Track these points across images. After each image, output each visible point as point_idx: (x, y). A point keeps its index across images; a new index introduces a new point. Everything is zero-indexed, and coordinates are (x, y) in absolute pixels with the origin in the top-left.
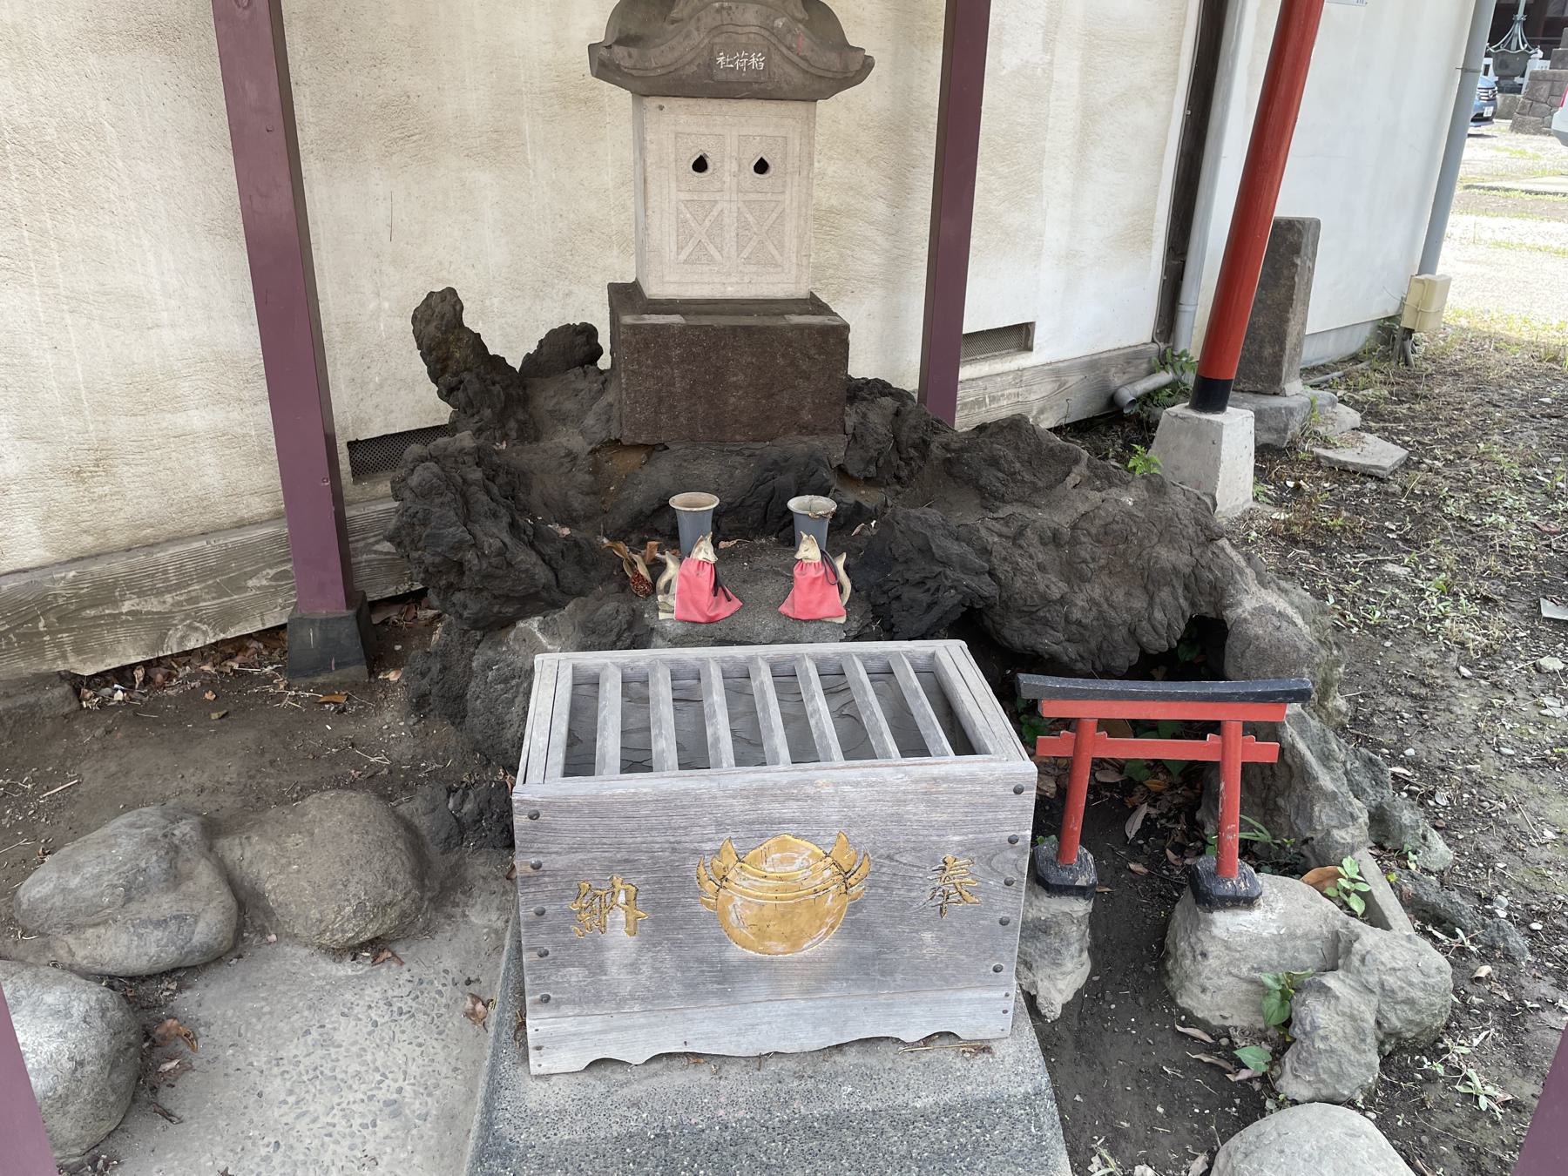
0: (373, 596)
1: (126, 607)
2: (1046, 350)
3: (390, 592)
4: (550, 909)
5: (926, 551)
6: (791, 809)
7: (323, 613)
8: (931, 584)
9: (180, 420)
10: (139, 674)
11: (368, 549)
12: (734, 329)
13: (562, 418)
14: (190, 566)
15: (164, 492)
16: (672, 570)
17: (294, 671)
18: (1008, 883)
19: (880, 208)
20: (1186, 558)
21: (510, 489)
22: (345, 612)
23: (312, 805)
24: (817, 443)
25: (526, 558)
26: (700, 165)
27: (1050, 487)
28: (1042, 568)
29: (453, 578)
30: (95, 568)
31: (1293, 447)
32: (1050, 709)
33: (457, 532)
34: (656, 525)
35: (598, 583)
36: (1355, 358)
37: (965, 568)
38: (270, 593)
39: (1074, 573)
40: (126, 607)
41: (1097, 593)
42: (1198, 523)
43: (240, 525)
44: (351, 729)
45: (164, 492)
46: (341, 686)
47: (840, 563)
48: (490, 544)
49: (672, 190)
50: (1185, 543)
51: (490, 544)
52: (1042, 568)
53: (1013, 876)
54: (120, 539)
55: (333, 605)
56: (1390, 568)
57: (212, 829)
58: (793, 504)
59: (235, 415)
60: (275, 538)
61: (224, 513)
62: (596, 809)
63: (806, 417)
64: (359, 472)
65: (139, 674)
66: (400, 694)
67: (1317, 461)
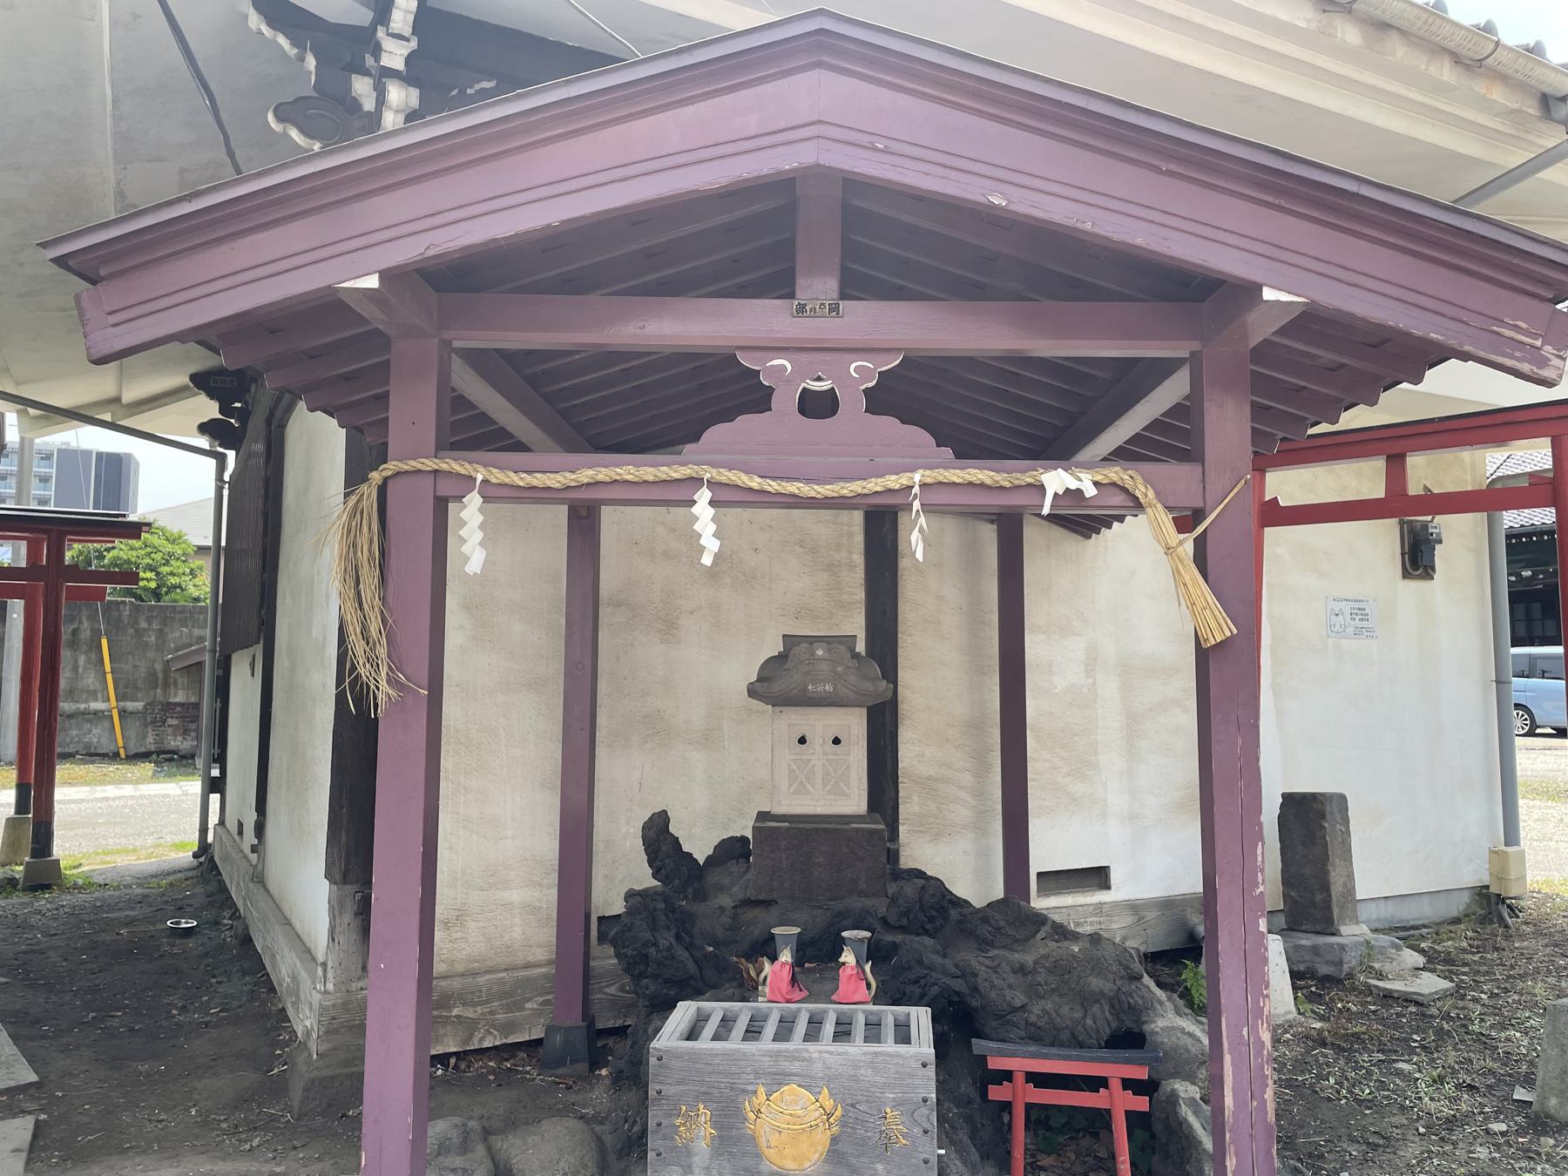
0: (600, 1025)
1: (455, 1012)
2: (1122, 889)
3: (610, 1024)
4: (665, 1122)
5: (920, 962)
6: (795, 1067)
7: (567, 1024)
8: (923, 982)
9: (506, 894)
10: (453, 1061)
11: (600, 990)
12: (817, 830)
13: (721, 889)
14: (495, 989)
15: (489, 940)
16: (768, 968)
17: (545, 1066)
18: (926, 1132)
19: (967, 778)
20: (1110, 985)
21: (683, 925)
22: (581, 1023)
23: (545, 1124)
24: (869, 902)
25: (683, 954)
26: (802, 741)
27: (1027, 939)
28: (1010, 987)
29: (642, 967)
30: (443, 983)
31: (1350, 976)
32: (995, 1063)
33: (647, 935)
34: (766, 948)
35: (722, 972)
36: (1456, 921)
37: (944, 973)
38: (537, 1013)
39: (1034, 992)
40: (455, 1012)
41: (1049, 1006)
42: (1121, 964)
43: (527, 966)
44: (572, 1097)
45: (489, 940)
46: (571, 1076)
47: (868, 967)
48: (664, 943)
49: (788, 754)
50: (1111, 977)
51: (664, 943)
52: (1010, 987)
53: (927, 1126)
54: (460, 968)
55: (574, 1019)
56: (1401, 1065)
57: (487, 1133)
58: (845, 934)
59: (536, 894)
60: (545, 976)
61: (520, 958)
62: (693, 1057)
63: (863, 886)
64: (602, 938)
65: (453, 1061)
66: (607, 1081)
67: (1369, 990)
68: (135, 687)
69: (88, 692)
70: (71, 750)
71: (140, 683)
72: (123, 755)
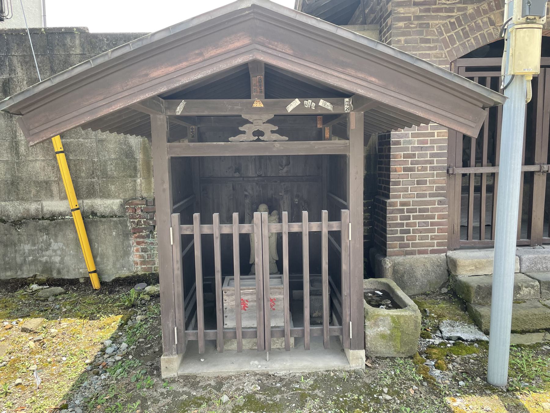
68: (104, 174)
69: (38, 184)
70: (25, 274)
71: (110, 168)
72: (96, 284)
